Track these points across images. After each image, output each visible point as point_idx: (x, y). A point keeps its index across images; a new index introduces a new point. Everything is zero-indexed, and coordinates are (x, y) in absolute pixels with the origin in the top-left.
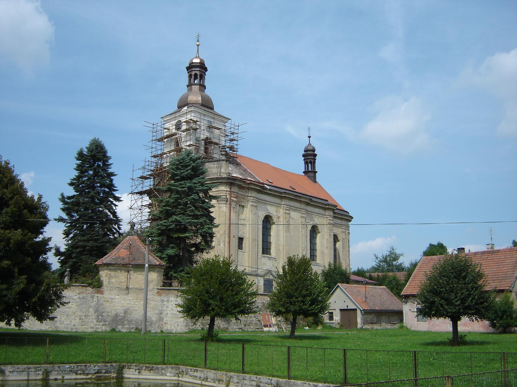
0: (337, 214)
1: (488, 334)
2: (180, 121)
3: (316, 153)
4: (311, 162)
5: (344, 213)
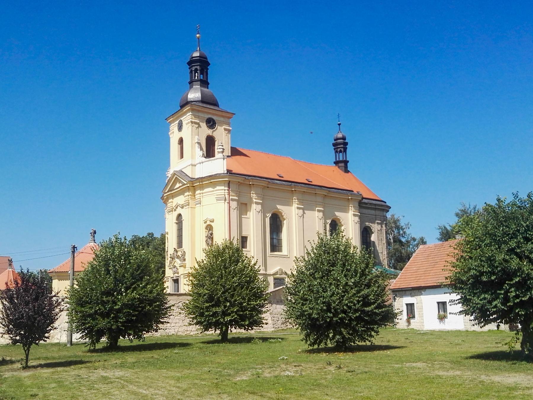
0: (369, 204)
1: (403, 347)
2: (181, 120)
5: (383, 203)
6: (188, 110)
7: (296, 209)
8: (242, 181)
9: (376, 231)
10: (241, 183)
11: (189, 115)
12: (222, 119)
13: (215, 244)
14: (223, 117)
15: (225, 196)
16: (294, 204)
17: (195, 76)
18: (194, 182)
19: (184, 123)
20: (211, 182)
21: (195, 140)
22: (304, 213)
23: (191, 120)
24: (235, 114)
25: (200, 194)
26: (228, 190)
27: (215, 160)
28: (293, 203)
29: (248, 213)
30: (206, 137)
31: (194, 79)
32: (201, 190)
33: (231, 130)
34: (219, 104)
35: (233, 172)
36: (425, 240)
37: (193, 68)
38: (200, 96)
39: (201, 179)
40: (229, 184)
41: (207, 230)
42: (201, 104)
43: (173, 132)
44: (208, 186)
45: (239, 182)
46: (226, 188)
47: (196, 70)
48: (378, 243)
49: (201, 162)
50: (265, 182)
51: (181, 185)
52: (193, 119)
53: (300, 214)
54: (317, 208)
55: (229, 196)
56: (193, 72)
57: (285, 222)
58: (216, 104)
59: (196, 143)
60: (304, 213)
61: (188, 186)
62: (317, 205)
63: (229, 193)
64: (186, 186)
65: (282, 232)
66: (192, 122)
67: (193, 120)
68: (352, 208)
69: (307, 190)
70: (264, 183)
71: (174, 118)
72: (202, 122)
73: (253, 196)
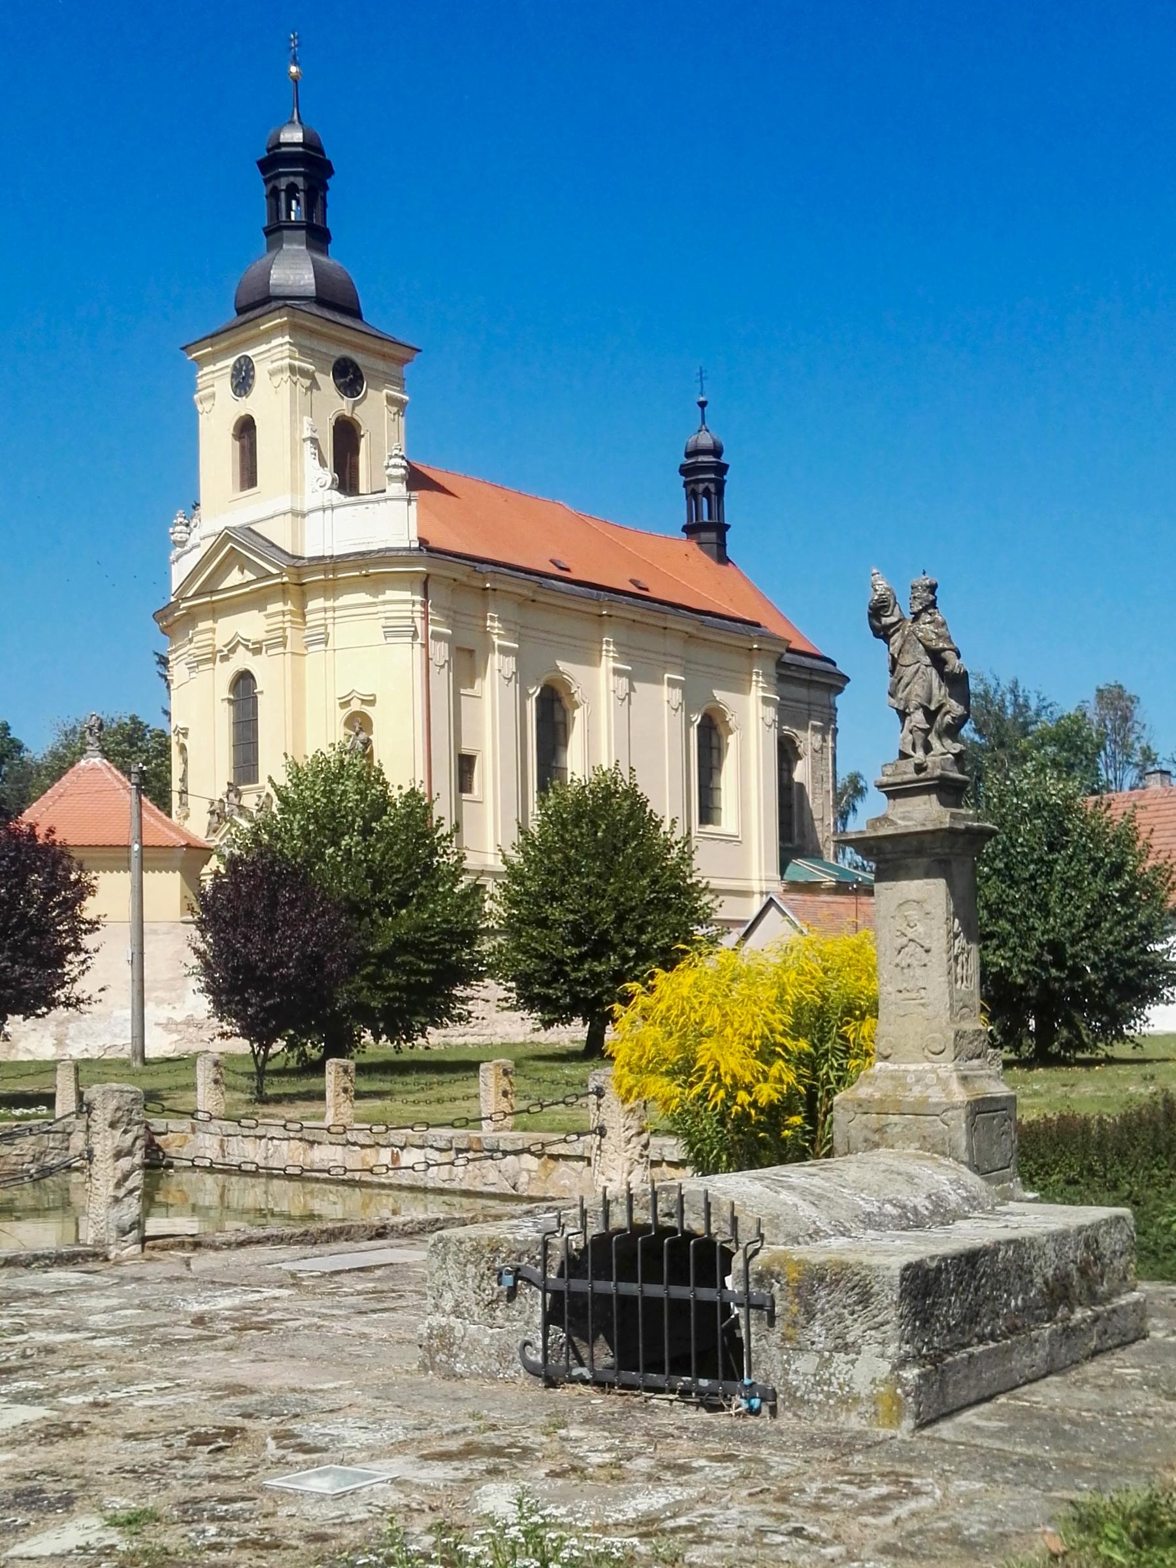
2: (246, 357)
3: (724, 459)
4: (707, 492)
6: (281, 325)
7: (611, 675)
8: (465, 579)
9: (809, 753)
10: (463, 585)
11: (282, 345)
12: (381, 365)
13: (572, 781)
14: (384, 356)
15: (413, 621)
16: (604, 658)
17: (289, 209)
18: (305, 570)
19: (261, 371)
20: (366, 576)
21: (302, 432)
22: (632, 688)
23: (288, 361)
24: (419, 351)
25: (325, 610)
26: (424, 604)
27: (378, 502)
28: (601, 656)
29: (478, 682)
30: (333, 421)
31: (284, 218)
32: (326, 599)
33: (407, 402)
34: (363, 312)
35: (431, 544)
36: (862, 783)
37: (283, 183)
38: (313, 281)
39: (331, 563)
40: (425, 586)
41: (353, 729)
42: (315, 309)
43: (213, 396)
44: (352, 586)
45: (455, 580)
46: (418, 598)
47: (292, 190)
48: (814, 789)
49: (327, 504)
50: (529, 583)
51: (249, 576)
52: (295, 359)
53: (622, 694)
54: (666, 676)
55: (427, 624)
56: (283, 195)
57: (578, 713)
58: (356, 314)
59: (304, 440)
60: (632, 688)
61: (283, 584)
62: (668, 665)
63: (426, 613)
64: (279, 580)
65: (566, 746)
66: (292, 369)
67: (297, 363)
68: (761, 679)
69: (643, 615)
70: (525, 588)
71: (217, 347)
72: (322, 371)
73: (492, 627)
